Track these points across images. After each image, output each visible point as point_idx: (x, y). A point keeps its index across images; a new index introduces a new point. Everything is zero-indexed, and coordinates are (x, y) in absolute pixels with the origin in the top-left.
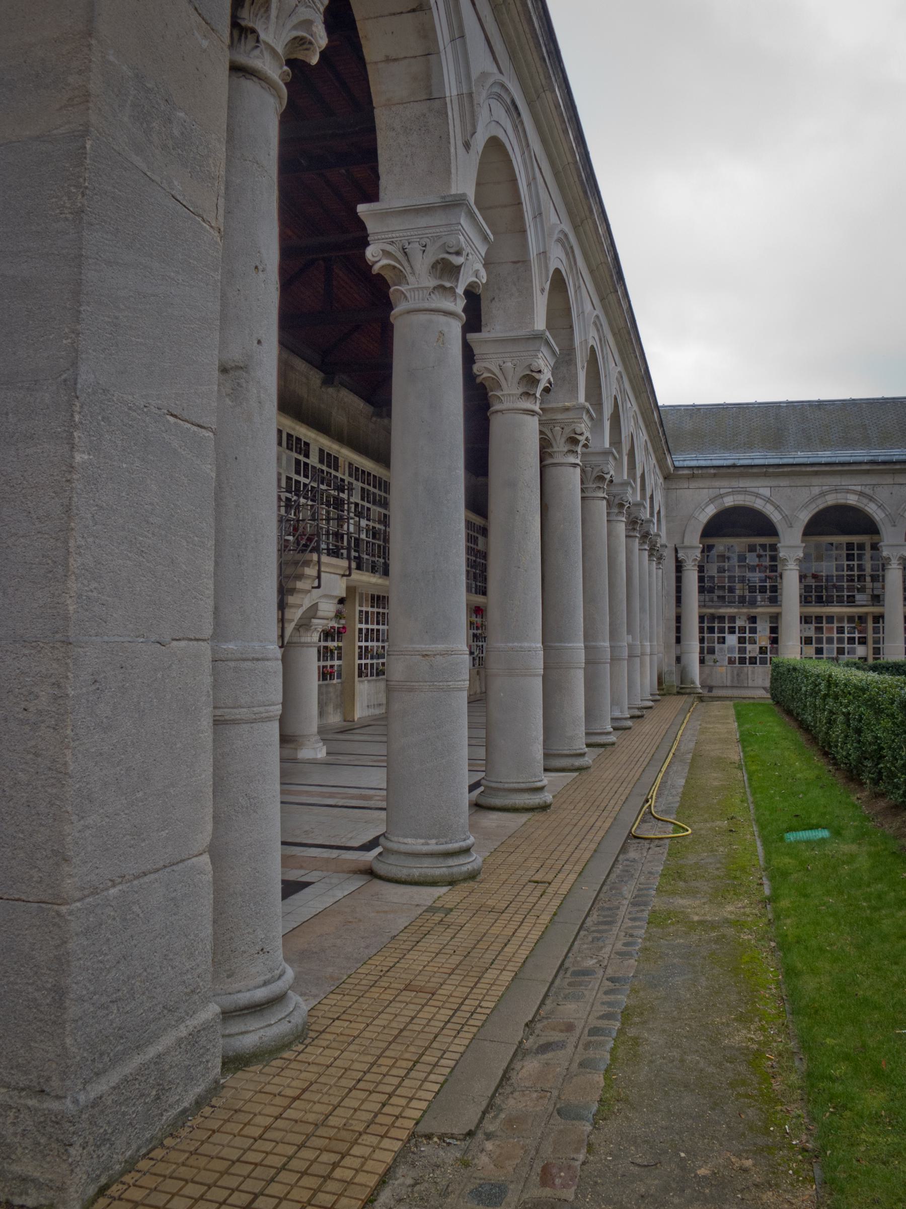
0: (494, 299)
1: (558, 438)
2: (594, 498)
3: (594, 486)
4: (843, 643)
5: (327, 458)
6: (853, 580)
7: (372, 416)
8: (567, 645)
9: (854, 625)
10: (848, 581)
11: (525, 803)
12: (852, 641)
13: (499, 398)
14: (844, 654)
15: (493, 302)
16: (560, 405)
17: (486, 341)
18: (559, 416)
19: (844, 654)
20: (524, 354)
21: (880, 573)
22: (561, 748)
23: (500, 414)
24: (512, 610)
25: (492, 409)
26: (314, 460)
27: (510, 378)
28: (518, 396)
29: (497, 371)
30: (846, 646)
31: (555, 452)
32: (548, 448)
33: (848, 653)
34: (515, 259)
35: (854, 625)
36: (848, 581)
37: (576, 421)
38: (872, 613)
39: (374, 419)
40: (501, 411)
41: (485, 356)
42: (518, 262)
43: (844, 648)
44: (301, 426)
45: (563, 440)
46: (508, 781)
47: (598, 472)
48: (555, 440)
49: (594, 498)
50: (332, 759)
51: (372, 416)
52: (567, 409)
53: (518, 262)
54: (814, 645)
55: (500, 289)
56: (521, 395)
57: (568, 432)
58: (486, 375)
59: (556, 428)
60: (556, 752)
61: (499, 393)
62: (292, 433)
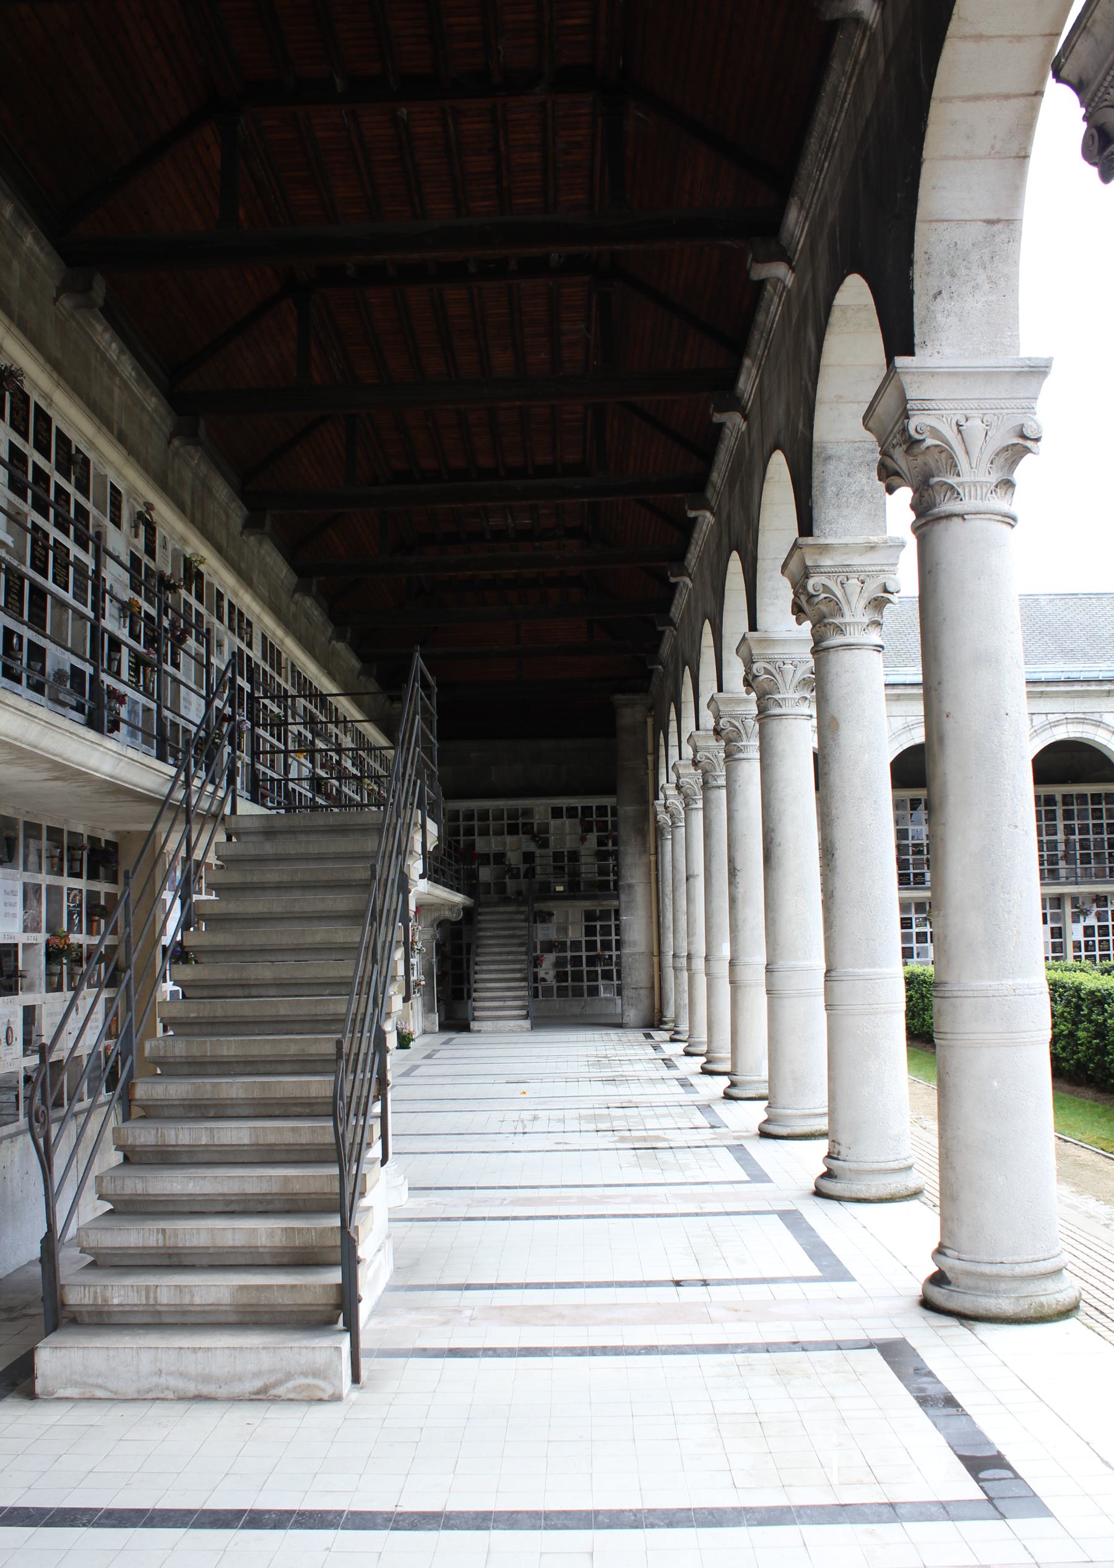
0: (940, 293)
1: (854, 599)
2: (797, 716)
3: (797, 696)
4: (910, 941)
5: (271, 652)
6: (920, 852)
7: (294, 592)
8: (856, 970)
9: (924, 916)
10: (914, 853)
11: (1042, 1305)
12: (923, 939)
13: (952, 488)
14: (912, 957)
15: (939, 299)
16: (861, 540)
17: (933, 374)
18: (856, 560)
19: (912, 957)
20: (1008, 404)
21: (1045, 838)
22: (882, 1158)
23: (956, 520)
24: (1009, 912)
25: (936, 510)
26: (256, 654)
27: (975, 452)
28: (993, 487)
29: (951, 435)
30: (914, 945)
31: (849, 624)
32: (832, 616)
33: (918, 956)
34: (992, 216)
35: (924, 916)
36: (914, 853)
37: (886, 568)
38: (1069, 894)
39: (297, 596)
40: (962, 516)
41: (933, 405)
42: (998, 221)
43: (912, 948)
44: (246, 591)
45: (863, 602)
46: (1017, 1258)
47: (804, 673)
48: (849, 602)
49: (797, 716)
50: (421, 1204)
51: (294, 592)
52: (872, 548)
53: (998, 221)
54: (584, 939)
55: (953, 275)
56: (996, 486)
57: (873, 589)
58: (930, 442)
59: (851, 581)
60: (875, 1166)
61: (952, 480)
62: (234, 601)
